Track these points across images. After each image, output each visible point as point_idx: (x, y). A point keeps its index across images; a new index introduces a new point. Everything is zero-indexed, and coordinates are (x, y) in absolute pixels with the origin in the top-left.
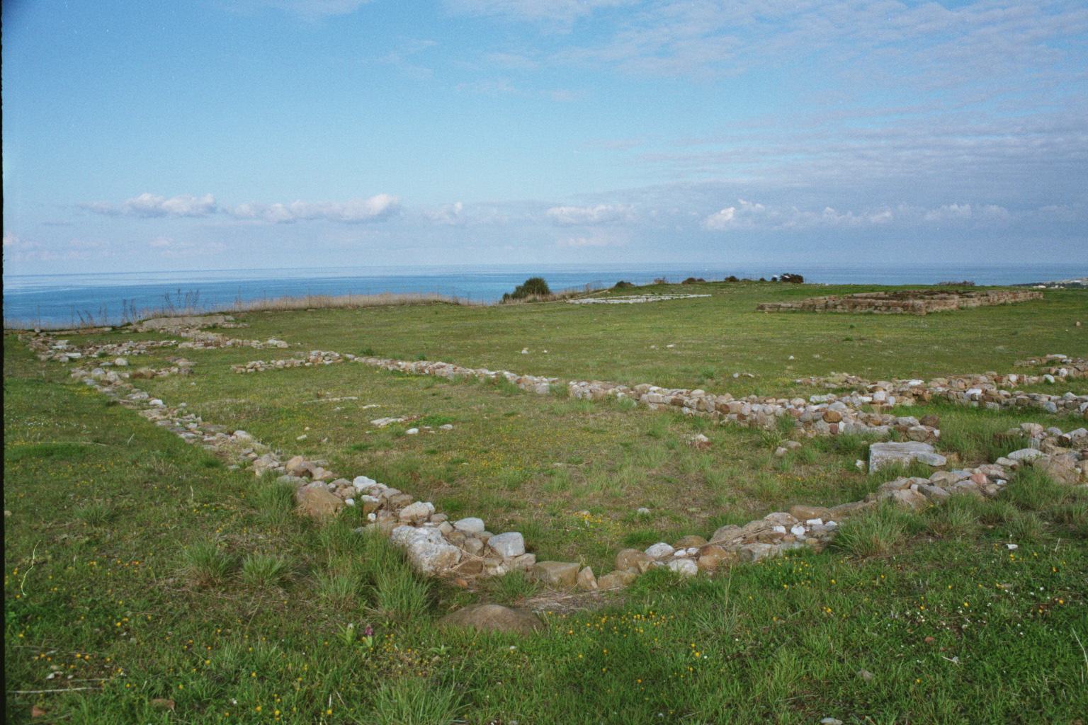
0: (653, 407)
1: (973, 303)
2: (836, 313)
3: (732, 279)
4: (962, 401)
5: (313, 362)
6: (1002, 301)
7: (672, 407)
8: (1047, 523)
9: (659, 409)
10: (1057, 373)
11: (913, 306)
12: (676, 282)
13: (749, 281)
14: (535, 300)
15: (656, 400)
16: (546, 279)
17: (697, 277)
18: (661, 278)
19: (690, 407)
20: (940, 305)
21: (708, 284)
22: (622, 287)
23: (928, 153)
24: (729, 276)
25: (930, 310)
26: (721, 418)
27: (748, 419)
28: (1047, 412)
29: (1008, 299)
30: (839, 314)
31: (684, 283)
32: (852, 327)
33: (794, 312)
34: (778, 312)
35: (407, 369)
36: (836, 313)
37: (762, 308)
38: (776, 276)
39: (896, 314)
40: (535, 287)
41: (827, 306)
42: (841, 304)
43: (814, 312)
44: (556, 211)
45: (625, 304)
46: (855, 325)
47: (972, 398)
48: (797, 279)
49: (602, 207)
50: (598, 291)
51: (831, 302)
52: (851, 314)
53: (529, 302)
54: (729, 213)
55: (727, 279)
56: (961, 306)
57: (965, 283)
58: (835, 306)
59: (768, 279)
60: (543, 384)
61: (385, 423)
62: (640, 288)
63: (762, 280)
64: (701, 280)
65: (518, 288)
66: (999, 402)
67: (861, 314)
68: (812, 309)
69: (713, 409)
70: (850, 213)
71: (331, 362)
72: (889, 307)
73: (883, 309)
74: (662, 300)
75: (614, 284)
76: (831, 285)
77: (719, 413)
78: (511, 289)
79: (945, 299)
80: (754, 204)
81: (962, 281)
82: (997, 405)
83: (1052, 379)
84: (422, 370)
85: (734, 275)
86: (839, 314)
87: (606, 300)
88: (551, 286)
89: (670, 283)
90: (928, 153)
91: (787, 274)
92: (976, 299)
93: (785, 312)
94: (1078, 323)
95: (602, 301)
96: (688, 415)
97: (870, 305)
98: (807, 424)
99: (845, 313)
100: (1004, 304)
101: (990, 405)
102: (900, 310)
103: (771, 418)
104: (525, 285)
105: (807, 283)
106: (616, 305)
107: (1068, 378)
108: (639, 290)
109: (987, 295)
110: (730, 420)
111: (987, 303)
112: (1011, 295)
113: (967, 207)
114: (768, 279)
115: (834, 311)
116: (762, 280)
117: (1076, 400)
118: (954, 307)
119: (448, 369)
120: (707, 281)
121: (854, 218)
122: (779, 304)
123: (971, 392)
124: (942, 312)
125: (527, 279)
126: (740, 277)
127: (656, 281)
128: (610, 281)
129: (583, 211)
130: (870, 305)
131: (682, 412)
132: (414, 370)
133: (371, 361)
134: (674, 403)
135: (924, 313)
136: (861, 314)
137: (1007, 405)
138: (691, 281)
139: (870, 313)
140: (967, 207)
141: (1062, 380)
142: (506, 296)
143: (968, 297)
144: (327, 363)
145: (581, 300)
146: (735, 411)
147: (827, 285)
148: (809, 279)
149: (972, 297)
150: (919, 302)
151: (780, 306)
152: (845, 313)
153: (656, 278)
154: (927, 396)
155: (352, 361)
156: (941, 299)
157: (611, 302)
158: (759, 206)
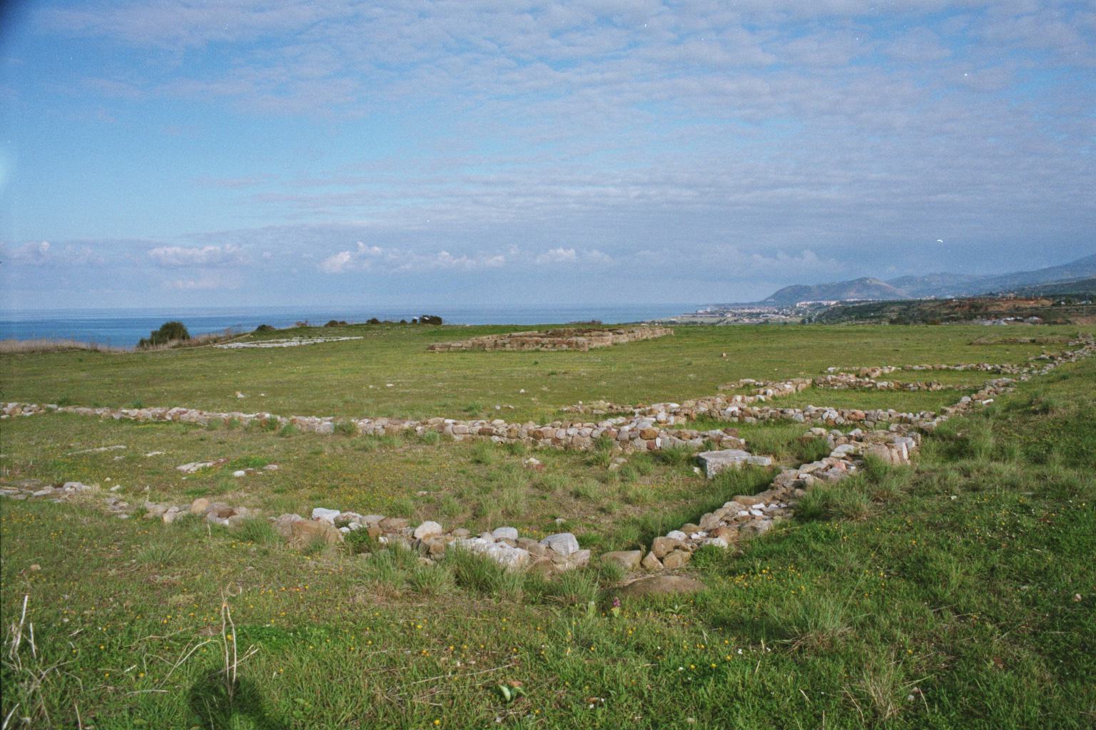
0: (458, 438)
1: (624, 339)
2: (505, 351)
3: (374, 321)
4: (724, 417)
5: (11, 415)
6: (645, 337)
7: (479, 437)
8: (268, 626)
9: (465, 439)
10: (765, 394)
11: (577, 343)
12: (317, 325)
13: (390, 323)
14: (179, 345)
15: (461, 431)
16: (185, 324)
17: (339, 320)
18: (303, 321)
19: (500, 436)
20: (598, 341)
21: (350, 327)
22: (264, 331)
23: (539, 200)
24: (370, 319)
25: (591, 347)
26: (535, 443)
27: (564, 442)
28: (797, 423)
29: (648, 334)
30: (509, 352)
31: (326, 326)
32: (536, 363)
33: (464, 351)
34: (448, 351)
35: (141, 417)
36: (505, 351)
37: (432, 348)
38: (415, 318)
39: (562, 351)
40: (172, 331)
41: (496, 345)
42: (510, 343)
43: (484, 350)
44: (160, 251)
45: (280, 348)
46: (537, 360)
47: (733, 414)
48: (436, 321)
49: (211, 248)
50: (240, 335)
51: (499, 342)
52: (520, 351)
53: (174, 347)
54: (345, 257)
55: (368, 321)
56: (615, 342)
57: (593, 321)
58: (504, 345)
59: (409, 320)
60: (324, 424)
61: (195, 469)
62: (283, 331)
63: (403, 322)
64: (343, 323)
65: (154, 334)
66: (756, 417)
67: (529, 352)
68: (481, 347)
69: (526, 436)
70: (465, 257)
71: (30, 413)
72: (555, 345)
73: (550, 346)
74: (315, 344)
75: (255, 328)
76: (471, 326)
77: (532, 439)
78: (147, 335)
79: (602, 335)
80: (370, 246)
81: (590, 321)
82: (754, 419)
83: (763, 398)
84: (162, 416)
85: (375, 317)
86: (509, 352)
87: (258, 344)
88: (191, 330)
89: (312, 326)
90: (539, 200)
91: (427, 316)
92: (625, 336)
93: (455, 352)
94: (724, 355)
95: (253, 346)
96: (498, 443)
97: (537, 343)
98: (624, 443)
99: (514, 351)
100: (646, 340)
101: (749, 419)
102: (565, 347)
103: (588, 440)
104: (161, 329)
105: (446, 324)
106: (269, 348)
107: (774, 397)
108: (284, 334)
109: (633, 332)
110: (546, 445)
111: (633, 340)
112: (651, 332)
113: (572, 251)
114: (409, 320)
115: (503, 349)
116: (403, 322)
117: (817, 411)
118: (609, 343)
119: (194, 414)
120: (349, 323)
121: (469, 261)
122: (448, 343)
123: (730, 409)
124: (601, 348)
125: (164, 323)
126: (381, 320)
127: (298, 324)
128: (253, 326)
129: (189, 252)
130: (537, 343)
131: (491, 441)
132: (150, 417)
133: (70, 409)
134: (481, 433)
135: (587, 349)
136: (529, 352)
137: (762, 418)
138: (333, 324)
139: (537, 351)
140: (572, 251)
141: (770, 399)
142: (142, 342)
143: (618, 333)
144: (28, 414)
145: (230, 345)
146: (549, 435)
147: (468, 325)
148: (447, 320)
149: (621, 334)
150: (581, 339)
151: (449, 347)
152: (514, 351)
153: (296, 321)
154: (694, 416)
155: (56, 412)
156: (599, 336)
157: (263, 346)
158: (376, 249)
